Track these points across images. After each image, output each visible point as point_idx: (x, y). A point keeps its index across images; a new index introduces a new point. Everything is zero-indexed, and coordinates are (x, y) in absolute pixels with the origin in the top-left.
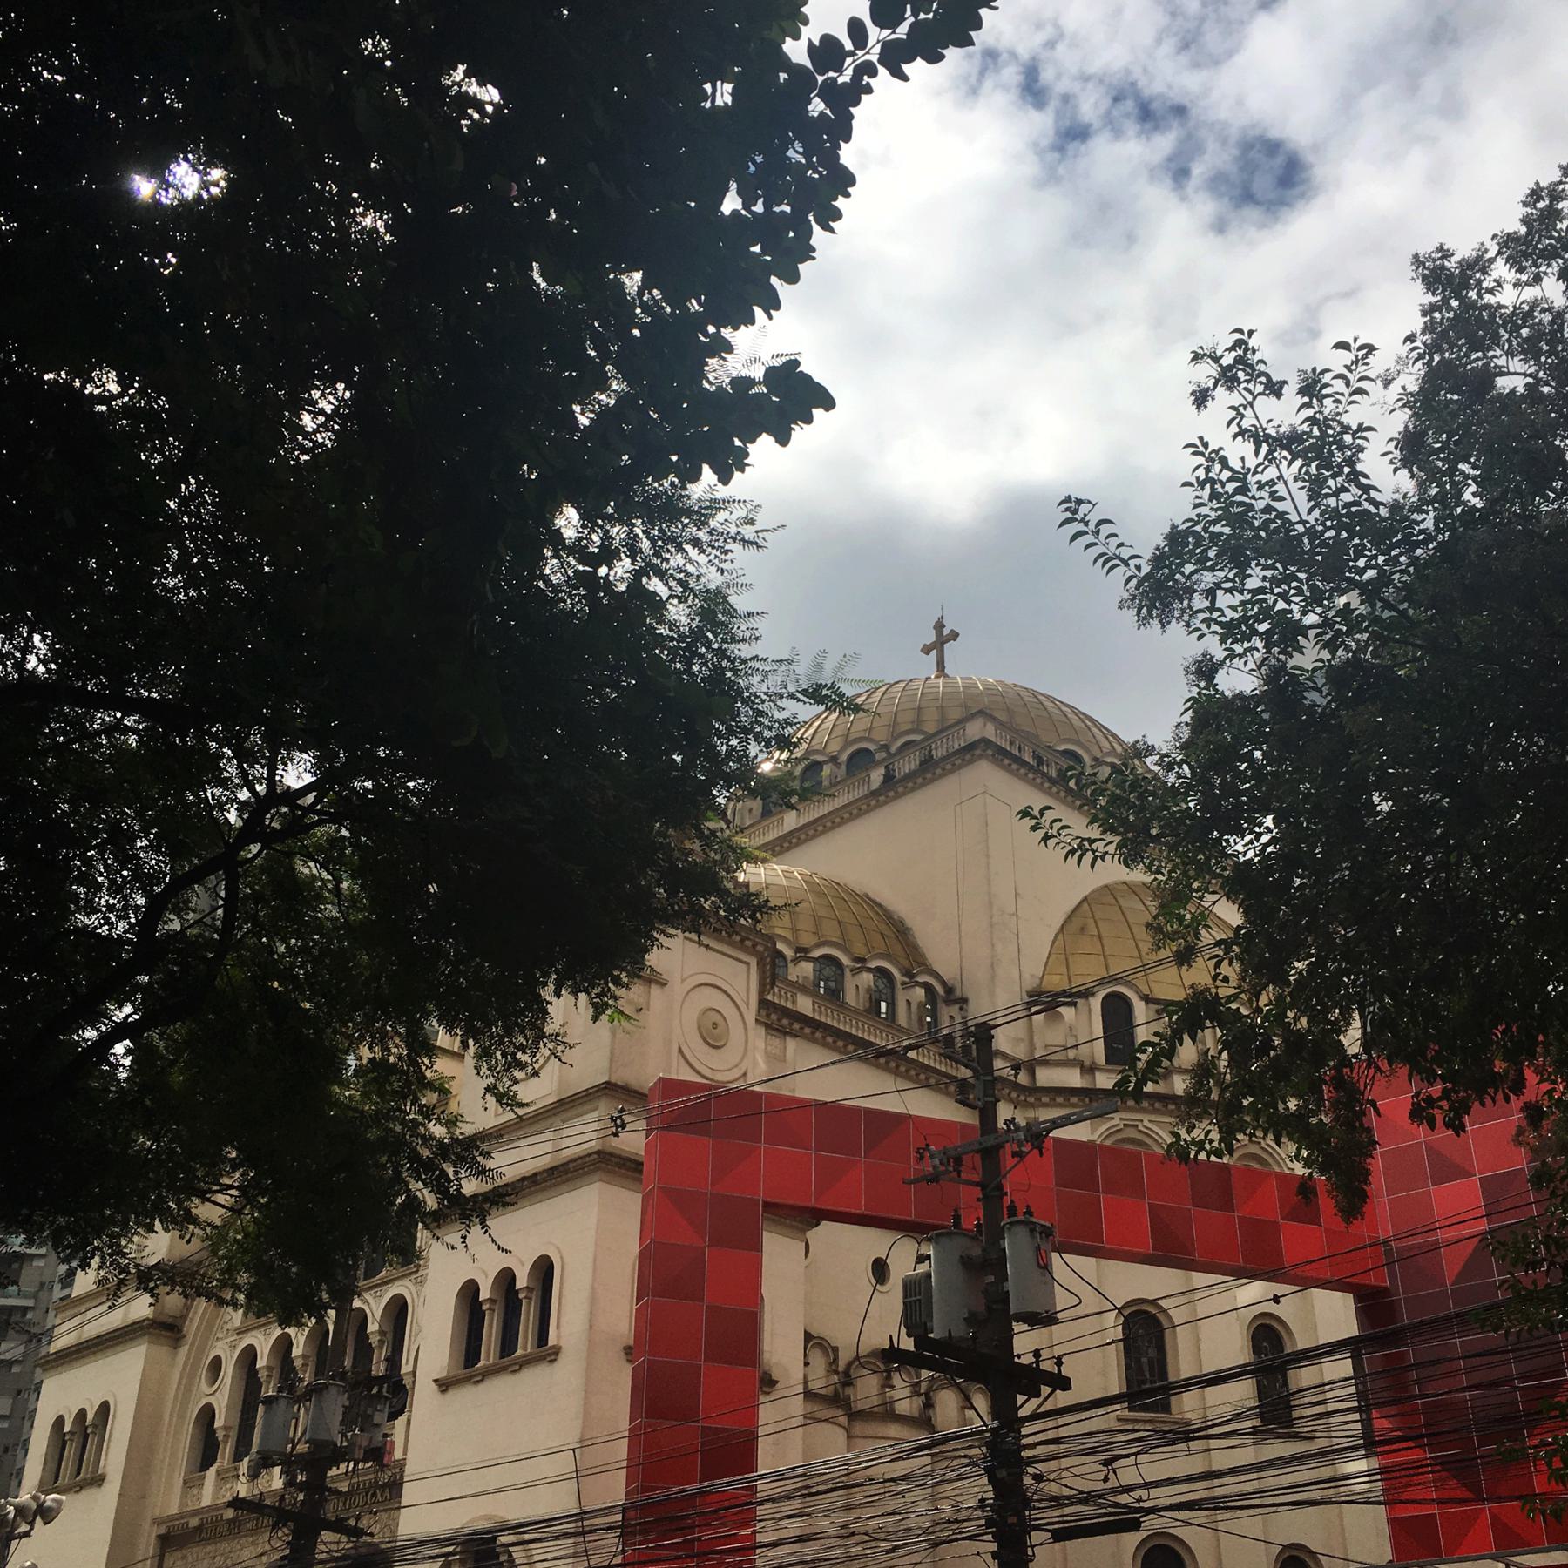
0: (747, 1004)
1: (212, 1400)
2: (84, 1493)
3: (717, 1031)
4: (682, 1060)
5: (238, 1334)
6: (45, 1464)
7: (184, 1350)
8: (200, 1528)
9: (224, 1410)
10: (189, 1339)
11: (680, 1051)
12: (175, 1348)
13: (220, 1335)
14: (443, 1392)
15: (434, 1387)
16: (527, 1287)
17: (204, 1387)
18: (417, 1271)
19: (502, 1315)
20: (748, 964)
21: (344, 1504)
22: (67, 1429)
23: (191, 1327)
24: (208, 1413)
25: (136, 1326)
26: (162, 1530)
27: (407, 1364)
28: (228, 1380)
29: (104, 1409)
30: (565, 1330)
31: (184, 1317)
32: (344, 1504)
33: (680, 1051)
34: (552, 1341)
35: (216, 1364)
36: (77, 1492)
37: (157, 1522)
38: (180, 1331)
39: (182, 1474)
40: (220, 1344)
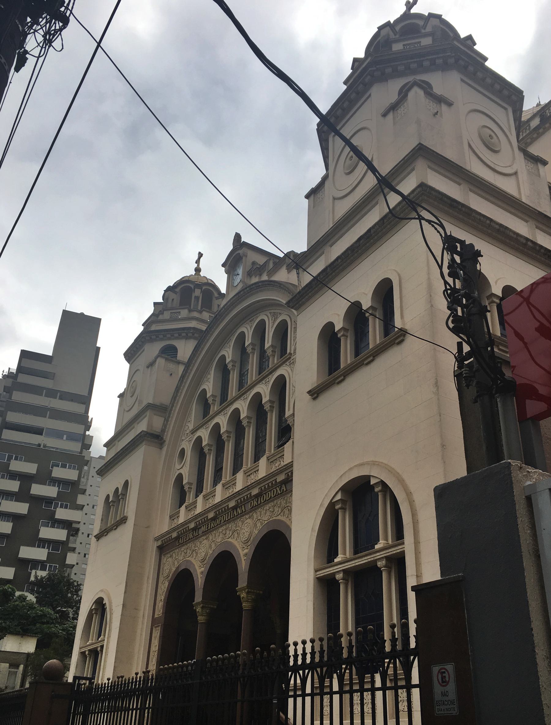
0: (510, 131)
1: (181, 471)
2: (118, 529)
3: (492, 140)
4: (470, 151)
5: (192, 434)
6: (102, 520)
7: (165, 448)
8: (177, 538)
9: (187, 474)
10: (167, 442)
11: (470, 146)
12: (161, 449)
13: (183, 438)
14: (314, 399)
15: (308, 397)
16: (371, 306)
17: (178, 466)
18: (290, 358)
19: (353, 339)
20: (506, 109)
21: (257, 502)
22: (110, 500)
23: (168, 437)
24: (180, 477)
25: (138, 437)
26: (159, 543)
27: (289, 410)
28: (189, 459)
29: (126, 484)
30: (408, 317)
31: (163, 431)
32: (257, 502)
33: (470, 146)
34: (398, 323)
35: (183, 452)
36: (115, 529)
37: (157, 539)
38: (162, 438)
39: (169, 513)
40: (184, 442)
